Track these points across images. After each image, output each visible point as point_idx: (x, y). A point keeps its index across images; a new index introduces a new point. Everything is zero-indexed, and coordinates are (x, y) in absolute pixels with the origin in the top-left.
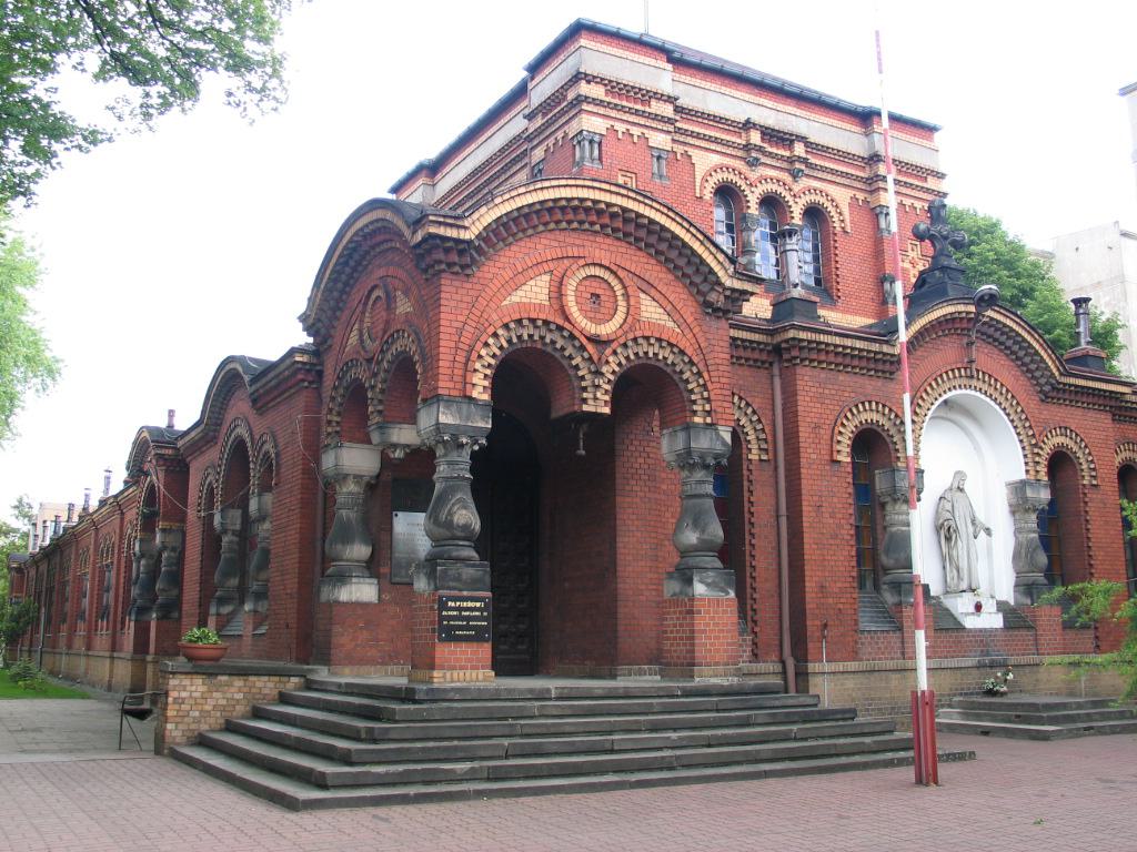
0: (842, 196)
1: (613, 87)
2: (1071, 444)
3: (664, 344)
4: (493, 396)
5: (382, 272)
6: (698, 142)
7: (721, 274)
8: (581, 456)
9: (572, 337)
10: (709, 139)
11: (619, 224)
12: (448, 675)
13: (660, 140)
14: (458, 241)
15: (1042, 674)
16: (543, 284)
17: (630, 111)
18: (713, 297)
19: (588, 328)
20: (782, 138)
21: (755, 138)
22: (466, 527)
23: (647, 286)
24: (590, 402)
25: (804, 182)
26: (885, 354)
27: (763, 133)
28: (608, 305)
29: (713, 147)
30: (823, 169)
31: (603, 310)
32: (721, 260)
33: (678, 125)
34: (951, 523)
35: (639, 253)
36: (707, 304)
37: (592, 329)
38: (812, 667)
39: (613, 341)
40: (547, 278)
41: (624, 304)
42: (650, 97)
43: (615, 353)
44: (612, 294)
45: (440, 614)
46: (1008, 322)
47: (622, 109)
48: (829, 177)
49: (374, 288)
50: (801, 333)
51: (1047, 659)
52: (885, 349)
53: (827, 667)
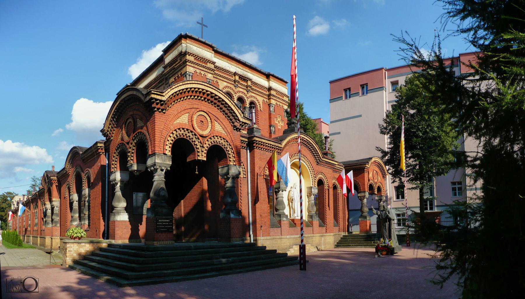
0: (260, 99)
1: (197, 57)
2: (323, 177)
3: (222, 138)
4: (172, 154)
5: (131, 113)
7: (239, 116)
8: (197, 174)
9: (195, 135)
10: (224, 77)
11: (209, 97)
12: (159, 243)
13: (210, 76)
14: (161, 101)
15: (314, 239)
16: (186, 117)
17: (201, 66)
18: (236, 124)
19: (200, 132)
20: (243, 78)
21: (237, 78)
22: (164, 196)
23: (217, 119)
24: (200, 156)
25: (250, 94)
26: (279, 147)
27: (239, 77)
28: (205, 125)
29: (225, 80)
30: (256, 90)
31: (204, 126)
32: (240, 112)
33: (215, 72)
34: (293, 198)
36: (235, 126)
37: (201, 132)
38: (258, 238)
39: (207, 137)
40: (187, 115)
41: (211, 125)
42: (207, 62)
43: (208, 141)
44: (206, 121)
45: (156, 224)
46: (311, 141)
47: (198, 65)
48: (257, 93)
49: (128, 119)
51: (315, 235)
52: (279, 145)
53: (262, 238)
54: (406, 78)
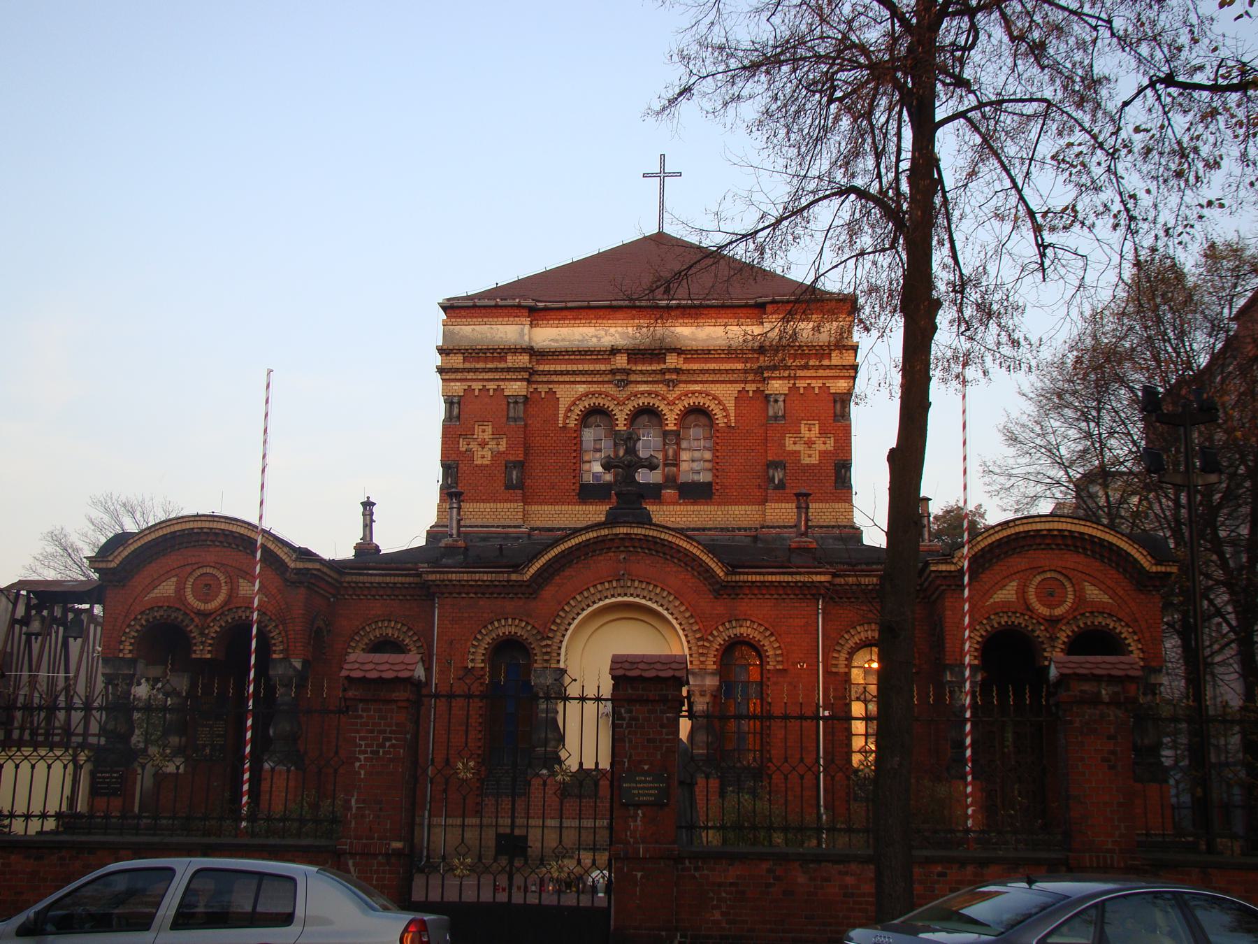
6: (561, 379)
16: (171, 583)
35: (240, 553)
40: (174, 579)
42: (506, 353)
47: (476, 370)
50: (430, 575)
54: (746, 334)
